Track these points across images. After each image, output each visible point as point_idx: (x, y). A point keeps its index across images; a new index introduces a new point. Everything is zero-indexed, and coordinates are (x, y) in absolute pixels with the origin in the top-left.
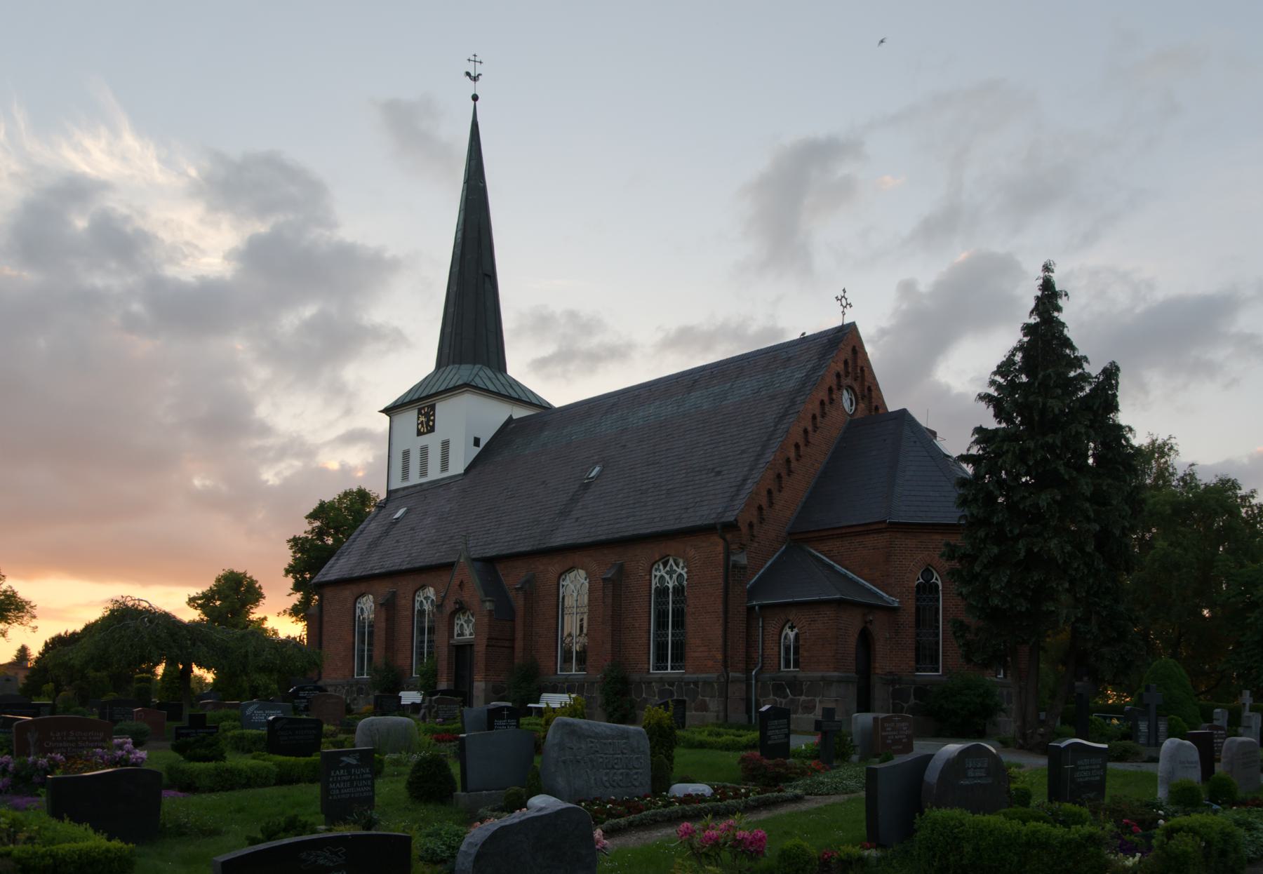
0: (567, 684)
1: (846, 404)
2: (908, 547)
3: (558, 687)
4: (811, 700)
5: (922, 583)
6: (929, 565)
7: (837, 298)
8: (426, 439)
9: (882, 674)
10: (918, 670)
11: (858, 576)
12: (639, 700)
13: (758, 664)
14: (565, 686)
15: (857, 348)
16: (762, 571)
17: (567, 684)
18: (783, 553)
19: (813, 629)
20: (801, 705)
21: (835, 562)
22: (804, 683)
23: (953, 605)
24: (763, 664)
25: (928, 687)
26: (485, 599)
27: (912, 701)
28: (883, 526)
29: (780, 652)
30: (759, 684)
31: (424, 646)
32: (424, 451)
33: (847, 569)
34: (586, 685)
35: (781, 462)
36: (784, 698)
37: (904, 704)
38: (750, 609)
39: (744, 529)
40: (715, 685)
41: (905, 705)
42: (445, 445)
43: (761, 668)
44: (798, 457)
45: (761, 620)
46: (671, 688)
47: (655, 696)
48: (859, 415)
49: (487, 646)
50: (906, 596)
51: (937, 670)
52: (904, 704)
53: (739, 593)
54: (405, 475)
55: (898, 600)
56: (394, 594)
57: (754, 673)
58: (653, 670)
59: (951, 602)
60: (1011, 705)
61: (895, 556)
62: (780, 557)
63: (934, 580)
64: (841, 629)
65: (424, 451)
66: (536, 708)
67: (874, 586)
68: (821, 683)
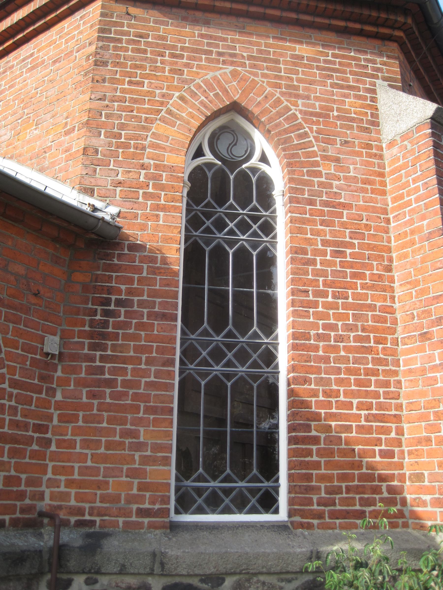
2: (165, 47)
5: (210, 165)
50: (147, 196)
61: (117, 64)
63: (254, 161)
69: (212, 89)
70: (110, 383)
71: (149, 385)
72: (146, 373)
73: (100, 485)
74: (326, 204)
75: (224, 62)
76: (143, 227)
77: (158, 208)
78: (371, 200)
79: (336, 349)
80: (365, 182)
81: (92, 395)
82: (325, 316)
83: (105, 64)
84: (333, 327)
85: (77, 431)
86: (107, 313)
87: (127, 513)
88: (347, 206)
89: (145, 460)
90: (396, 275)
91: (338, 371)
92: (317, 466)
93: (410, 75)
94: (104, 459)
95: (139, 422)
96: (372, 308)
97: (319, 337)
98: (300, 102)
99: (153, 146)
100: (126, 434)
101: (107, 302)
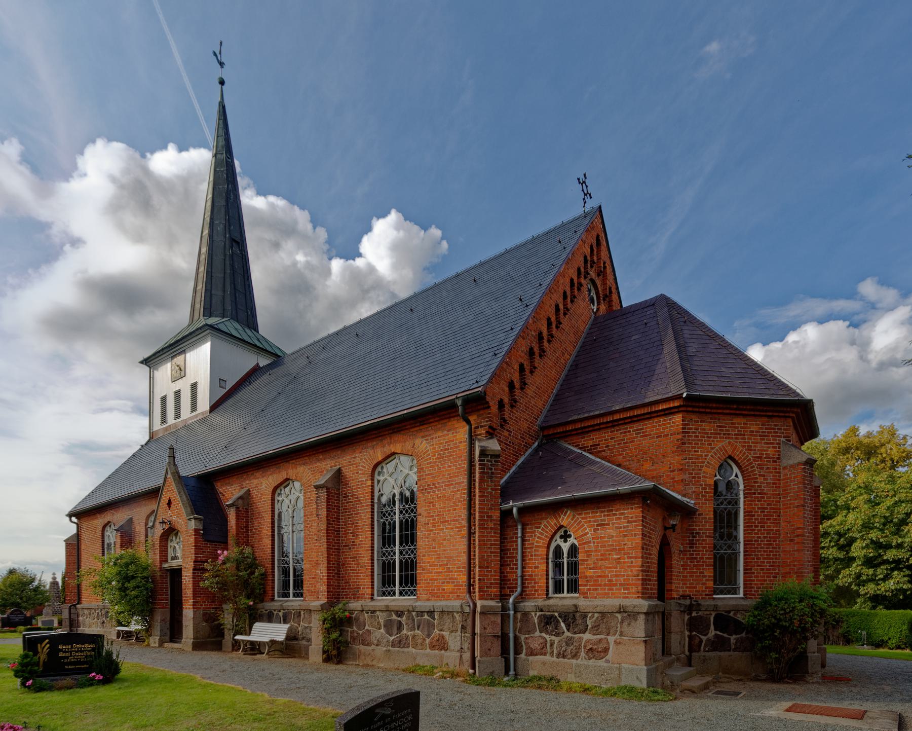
0: (282, 611)
2: (705, 433)
3: (273, 614)
4: (600, 640)
6: (730, 457)
8: (178, 385)
12: (361, 632)
13: (516, 588)
14: (281, 614)
16: (514, 469)
17: (282, 611)
18: (536, 451)
22: (590, 615)
23: (759, 508)
24: (523, 587)
25: (731, 614)
26: (189, 517)
27: (712, 632)
32: (178, 394)
34: (302, 613)
36: (557, 635)
37: (702, 637)
41: (704, 638)
42: (194, 386)
43: (521, 594)
45: (519, 527)
46: (399, 619)
47: (380, 629)
49: (194, 570)
50: (703, 496)
52: (702, 637)
53: (489, 490)
54: (164, 420)
56: (130, 521)
57: (511, 600)
58: (279, 597)
59: (756, 505)
61: (690, 443)
63: (733, 477)
65: (178, 394)
66: (243, 641)
68: (619, 616)
69: (722, 451)
71: (707, 558)
72: (705, 555)
73: (694, 588)
74: (759, 494)
75: (726, 438)
77: (706, 500)
78: (776, 491)
79: (760, 544)
80: (773, 484)
81: (691, 562)
82: (757, 534)
83: (685, 444)
84: (760, 537)
85: (688, 573)
87: (702, 595)
88: (766, 494)
89: (707, 580)
90: (781, 518)
91: (761, 551)
92: (754, 580)
93: (278, 466)
94: (696, 580)
96: (772, 530)
97: (755, 541)
98: (752, 452)
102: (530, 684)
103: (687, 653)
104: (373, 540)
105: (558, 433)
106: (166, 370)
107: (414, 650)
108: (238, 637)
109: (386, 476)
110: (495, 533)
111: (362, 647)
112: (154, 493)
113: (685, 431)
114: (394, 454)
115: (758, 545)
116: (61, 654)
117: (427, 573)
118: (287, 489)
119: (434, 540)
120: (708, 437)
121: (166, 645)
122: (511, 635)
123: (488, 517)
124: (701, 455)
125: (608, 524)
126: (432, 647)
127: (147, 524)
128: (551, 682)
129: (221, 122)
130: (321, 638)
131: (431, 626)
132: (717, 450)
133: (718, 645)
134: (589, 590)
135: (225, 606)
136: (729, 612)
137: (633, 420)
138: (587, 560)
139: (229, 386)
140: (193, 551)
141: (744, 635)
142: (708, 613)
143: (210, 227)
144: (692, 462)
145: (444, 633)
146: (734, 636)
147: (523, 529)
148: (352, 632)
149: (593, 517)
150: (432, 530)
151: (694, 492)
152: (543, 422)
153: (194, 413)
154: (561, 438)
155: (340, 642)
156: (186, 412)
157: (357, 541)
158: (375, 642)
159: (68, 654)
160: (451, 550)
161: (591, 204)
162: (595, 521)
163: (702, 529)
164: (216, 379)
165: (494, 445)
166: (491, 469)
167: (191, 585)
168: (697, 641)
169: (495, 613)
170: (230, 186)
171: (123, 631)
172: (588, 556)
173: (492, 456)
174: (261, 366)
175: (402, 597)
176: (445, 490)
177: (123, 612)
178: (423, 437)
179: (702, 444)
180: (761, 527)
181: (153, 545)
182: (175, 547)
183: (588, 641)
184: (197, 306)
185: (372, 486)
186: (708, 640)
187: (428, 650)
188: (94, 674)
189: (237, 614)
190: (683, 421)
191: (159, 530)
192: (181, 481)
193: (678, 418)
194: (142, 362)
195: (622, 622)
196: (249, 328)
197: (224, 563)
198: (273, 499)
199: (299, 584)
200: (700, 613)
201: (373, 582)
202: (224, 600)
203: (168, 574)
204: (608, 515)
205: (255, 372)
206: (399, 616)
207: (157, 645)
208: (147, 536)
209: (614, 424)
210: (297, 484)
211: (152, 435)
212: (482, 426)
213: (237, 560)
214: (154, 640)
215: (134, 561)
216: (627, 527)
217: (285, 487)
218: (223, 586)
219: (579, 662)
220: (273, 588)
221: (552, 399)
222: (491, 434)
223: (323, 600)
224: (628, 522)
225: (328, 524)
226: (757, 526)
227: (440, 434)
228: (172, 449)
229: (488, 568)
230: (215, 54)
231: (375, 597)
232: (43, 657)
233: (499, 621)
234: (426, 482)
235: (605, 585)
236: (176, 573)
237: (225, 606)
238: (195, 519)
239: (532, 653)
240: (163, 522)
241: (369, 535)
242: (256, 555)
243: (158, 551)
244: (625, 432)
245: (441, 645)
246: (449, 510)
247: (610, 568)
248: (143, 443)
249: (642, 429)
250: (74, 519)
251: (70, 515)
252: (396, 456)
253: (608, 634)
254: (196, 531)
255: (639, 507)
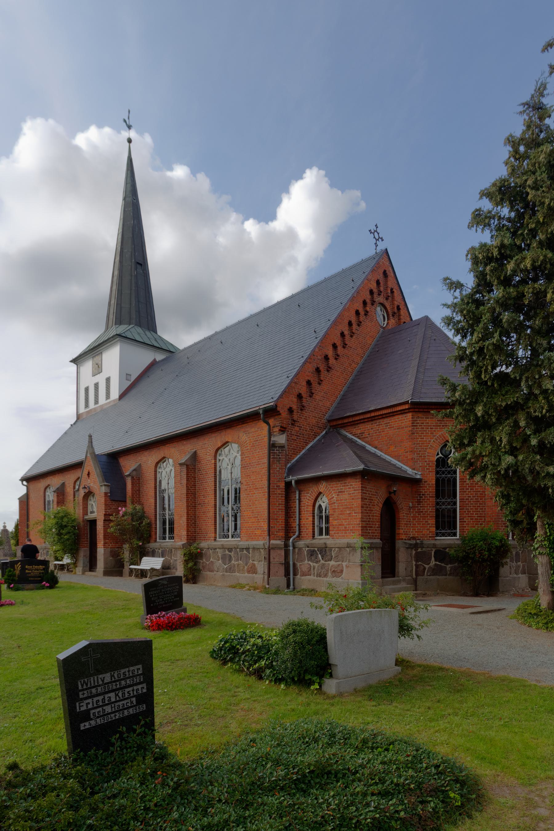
1: (380, 319)
2: (429, 426)
4: (339, 565)
5: (440, 457)
7: (370, 231)
9: (405, 539)
10: (437, 535)
11: (385, 454)
12: (208, 563)
13: (295, 532)
14: (160, 551)
15: (387, 272)
16: (304, 451)
18: (324, 437)
19: (341, 500)
20: (331, 569)
21: (366, 443)
22: (333, 549)
24: (300, 532)
25: (447, 550)
27: (433, 562)
28: (407, 407)
29: (313, 521)
30: (297, 550)
31: (169, 525)
32: (96, 386)
33: (376, 448)
35: (319, 357)
36: (317, 562)
38: (288, 485)
39: (284, 414)
40: (262, 551)
41: (427, 566)
42: (108, 380)
43: (298, 536)
44: (337, 357)
47: (219, 560)
48: (390, 327)
49: (104, 520)
50: (427, 469)
51: (455, 535)
54: (87, 405)
55: (420, 473)
56: (63, 485)
58: (160, 539)
60: (519, 563)
61: (417, 433)
62: (319, 440)
64: (366, 499)
65: (96, 386)
66: (135, 569)
67: (399, 461)
68: (348, 549)
70: (422, 512)
72: (429, 509)
76: (232, 569)
77: (430, 472)
86: (420, 497)
89: (430, 527)
92: (465, 527)
94: (422, 527)
95: (428, 519)
97: (467, 499)
99: (428, 456)
100: (426, 522)
101: (420, 495)
102: (299, 593)
103: (414, 576)
104: (215, 500)
105: (339, 424)
106: (88, 366)
107: (238, 574)
108: (132, 567)
109: (224, 457)
110: (281, 497)
111: (208, 573)
112: (78, 465)
113: (414, 424)
114: (227, 442)
115: (468, 502)
116: (27, 571)
117: (246, 523)
118: (165, 464)
119: (250, 501)
120: (431, 428)
121: (87, 573)
122: (291, 563)
123: (277, 486)
124: (426, 441)
125: (344, 492)
126: (249, 572)
127: (74, 488)
128: (312, 592)
129: (129, 172)
130: (183, 566)
131: (247, 558)
132: (438, 437)
133: (437, 571)
134: (335, 533)
135: (124, 546)
136: (445, 548)
137: (383, 417)
138: (333, 515)
139: (133, 378)
140: (103, 508)
141: (456, 564)
142: (430, 549)
143: (120, 255)
144: (419, 446)
145: (255, 562)
146: (450, 566)
147: (300, 494)
148: (203, 563)
149: (336, 487)
150: (249, 494)
151: (421, 466)
152: (330, 416)
153: (108, 401)
154: (342, 427)
155: (195, 570)
156: (102, 400)
157: (206, 501)
158: (216, 569)
159: (30, 571)
160: (260, 507)
161: (382, 246)
162: (338, 489)
163: (427, 492)
164: (124, 374)
165: (281, 439)
166: (279, 455)
167: (102, 531)
168: (422, 568)
169: (280, 549)
170: (135, 221)
171: (58, 564)
172: (334, 512)
173: (279, 447)
174: (157, 360)
175: (233, 539)
176: (256, 467)
177: (59, 551)
178: (244, 432)
179: (427, 433)
180: (471, 489)
181: (78, 503)
182: (92, 505)
183: (332, 566)
184: (111, 317)
185: (215, 464)
186: (430, 567)
187: (246, 574)
188: (44, 583)
189: (132, 551)
190: (412, 418)
191: (82, 493)
192: (97, 457)
193: (409, 415)
194: (71, 361)
195: (349, 554)
196: (149, 330)
197: (123, 516)
198: (156, 471)
199: (172, 530)
200: (424, 549)
201: (216, 529)
202: (124, 542)
203: (88, 524)
204: (344, 486)
205: (153, 364)
206: (230, 552)
207: (81, 573)
208: (74, 497)
209: (372, 419)
210: (171, 461)
211: (79, 416)
212: (277, 426)
213: (132, 514)
214: (79, 570)
215: (66, 515)
216: (354, 493)
217: (163, 463)
218: (123, 532)
219: (328, 579)
220: (156, 533)
221: (339, 398)
222: (283, 430)
223: (184, 541)
224: (354, 490)
225: (188, 489)
226: (468, 489)
227: (253, 430)
228: (90, 436)
229: (277, 519)
230: (125, 121)
231: (218, 539)
232: (17, 572)
233: (283, 554)
234: (246, 462)
235: (343, 530)
236: (93, 523)
237: (124, 546)
238: (105, 485)
239: (304, 574)
240: (85, 488)
241: (212, 496)
242: (145, 510)
243: (81, 508)
244: (379, 425)
245: (253, 570)
246: (259, 481)
247: (345, 519)
248: (72, 423)
249: (389, 423)
250: (25, 483)
251: (22, 480)
252: (229, 444)
253: (343, 562)
254: (106, 494)
255: (358, 482)
